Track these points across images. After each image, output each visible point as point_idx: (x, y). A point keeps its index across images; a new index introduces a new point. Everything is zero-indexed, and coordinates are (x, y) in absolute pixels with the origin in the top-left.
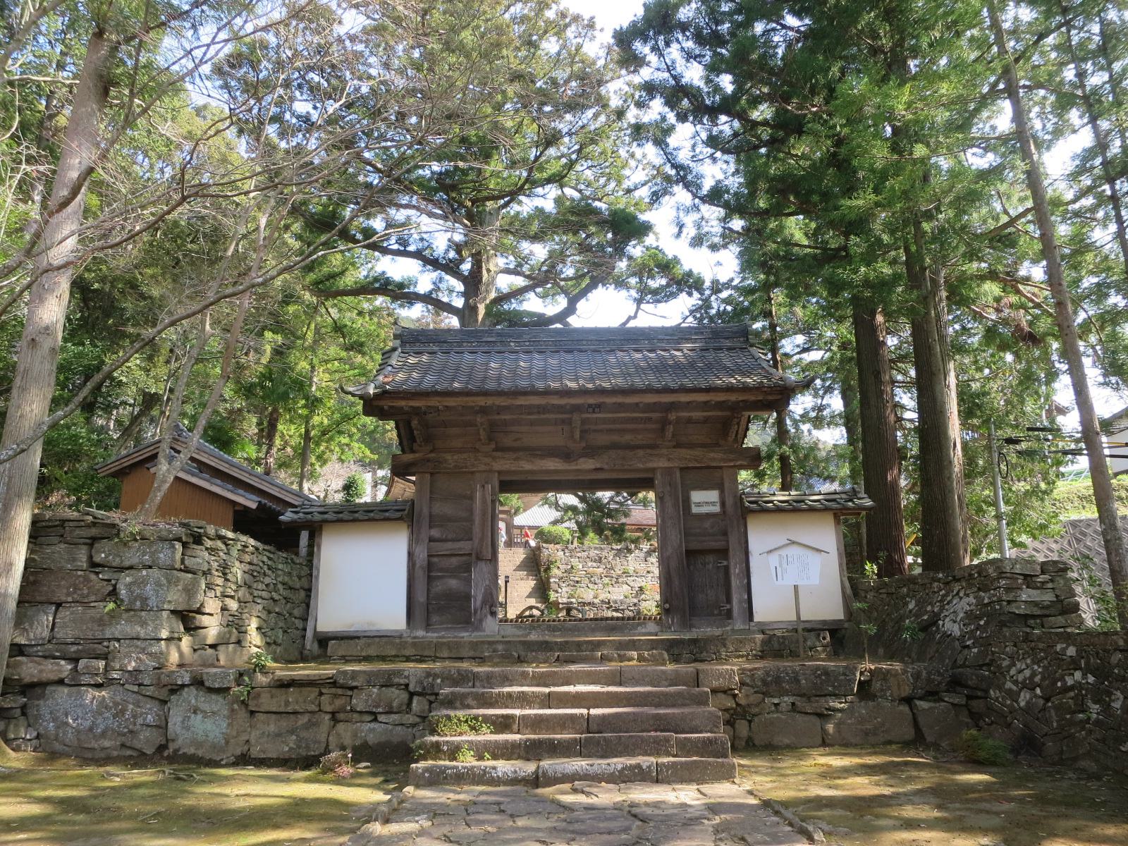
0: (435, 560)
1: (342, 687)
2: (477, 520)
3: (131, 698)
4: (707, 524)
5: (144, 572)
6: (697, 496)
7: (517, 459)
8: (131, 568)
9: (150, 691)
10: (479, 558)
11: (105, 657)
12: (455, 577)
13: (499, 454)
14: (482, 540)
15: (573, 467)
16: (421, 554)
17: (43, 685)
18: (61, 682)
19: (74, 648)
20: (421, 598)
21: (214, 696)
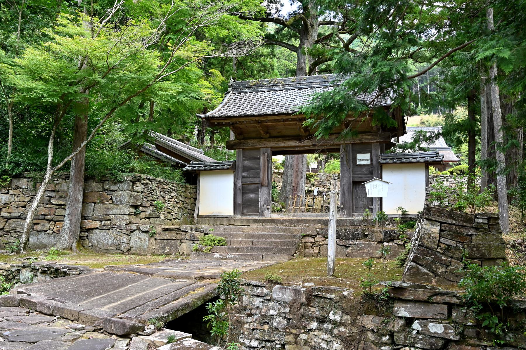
0: (245, 186)
1: (183, 231)
2: (262, 168)
3: (119, 233)
4: (364, 169)
5: (120, 192)
6: (359, 156)
7: (278, 141)
8: (116, 190)
9: (125, 232)
10: (262, 186)
11: (110, 220)
12: (253, 193)
13: (271, 139)
14: (263, 177)
15: (302, 144)
16: (239, 184)
17: (93, 229)
18: (97, 228)
19: (101, 217)
20: (239, 201)
21: (144, 234)
